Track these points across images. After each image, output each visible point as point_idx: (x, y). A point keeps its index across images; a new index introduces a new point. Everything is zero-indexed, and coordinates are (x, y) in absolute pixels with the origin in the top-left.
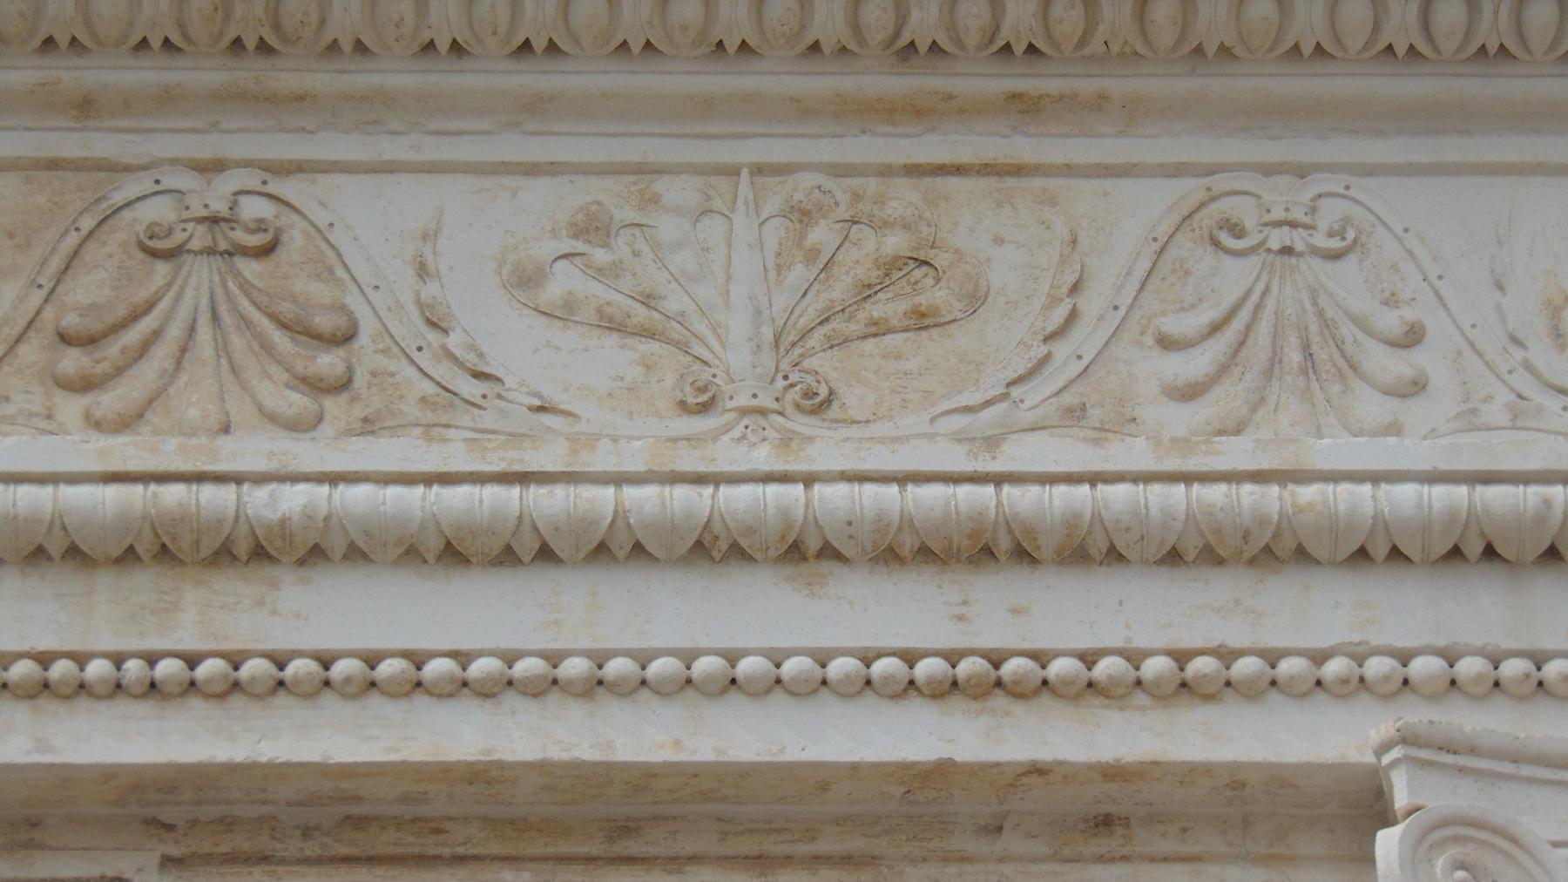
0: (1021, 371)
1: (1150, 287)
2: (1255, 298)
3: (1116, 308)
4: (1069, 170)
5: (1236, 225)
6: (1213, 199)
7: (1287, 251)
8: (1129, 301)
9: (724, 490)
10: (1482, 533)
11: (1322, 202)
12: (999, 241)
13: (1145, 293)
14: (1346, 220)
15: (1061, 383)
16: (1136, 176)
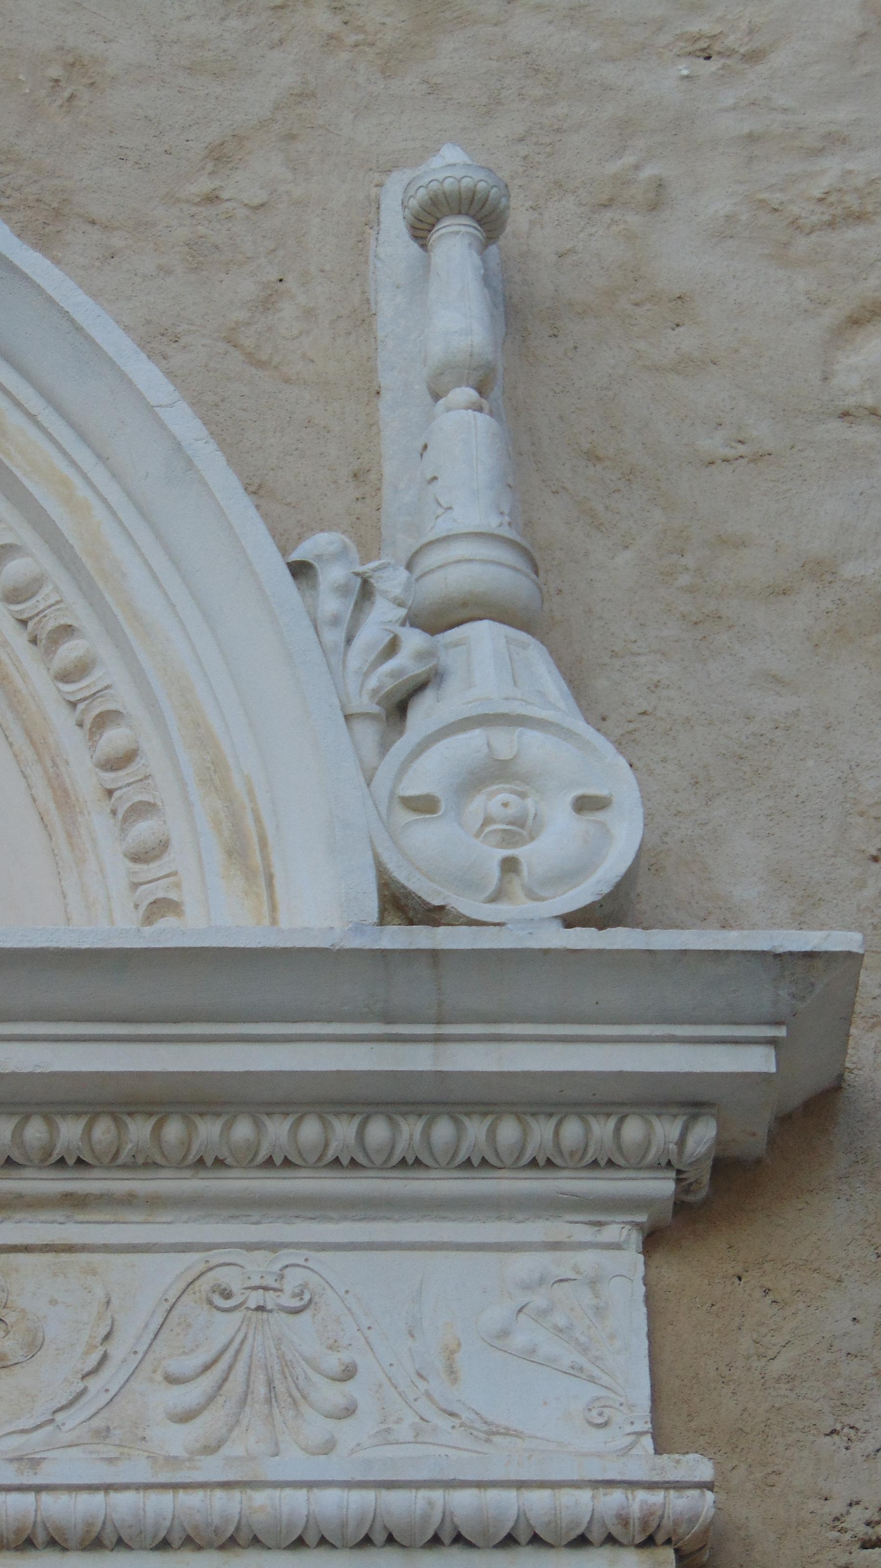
0: (64, 1402)
1: (161, 1336)
2: (235, 1345)
3: (135, 1352)
4: (107, 1248)
5: (225, 1290)
6: (210, 1269)
7: (260, 1309)
8: (145, 1347)
9: (45, 1497)
10: (385, 1527)
11: (287, 1271)
12: (53, 1302)
13: (158, 1341)
14: (304, 1287)
15: (93, 1410)
16: (155, 1252)
